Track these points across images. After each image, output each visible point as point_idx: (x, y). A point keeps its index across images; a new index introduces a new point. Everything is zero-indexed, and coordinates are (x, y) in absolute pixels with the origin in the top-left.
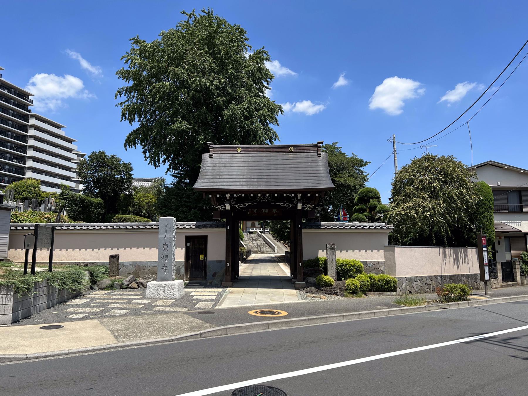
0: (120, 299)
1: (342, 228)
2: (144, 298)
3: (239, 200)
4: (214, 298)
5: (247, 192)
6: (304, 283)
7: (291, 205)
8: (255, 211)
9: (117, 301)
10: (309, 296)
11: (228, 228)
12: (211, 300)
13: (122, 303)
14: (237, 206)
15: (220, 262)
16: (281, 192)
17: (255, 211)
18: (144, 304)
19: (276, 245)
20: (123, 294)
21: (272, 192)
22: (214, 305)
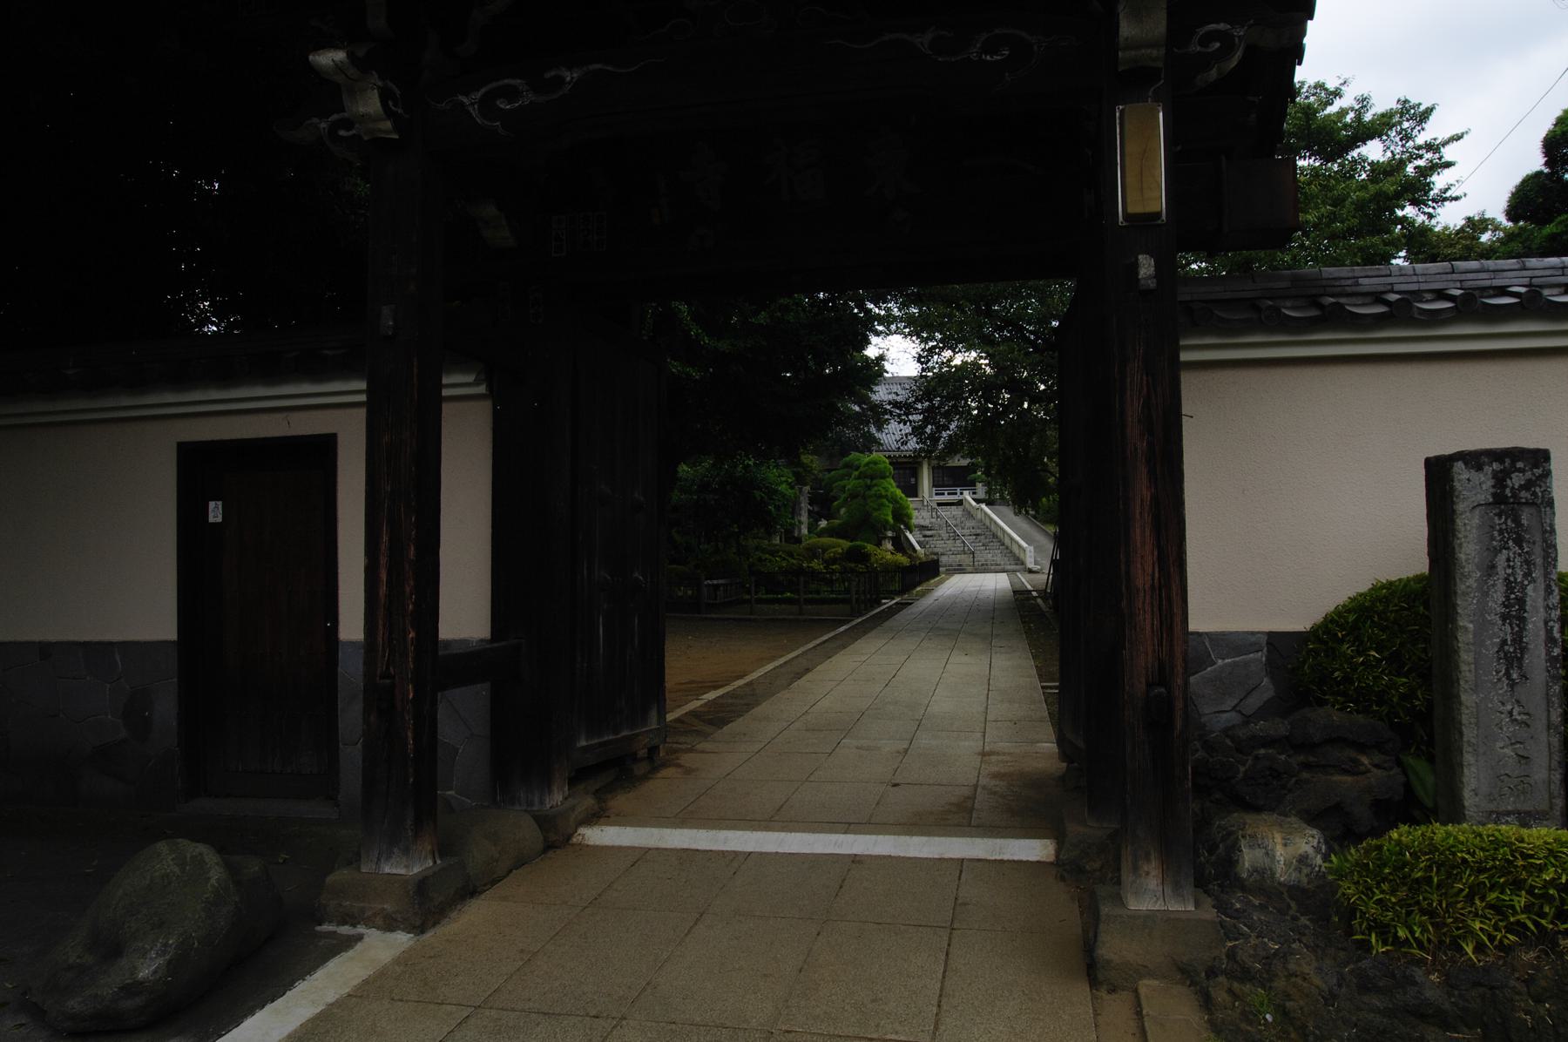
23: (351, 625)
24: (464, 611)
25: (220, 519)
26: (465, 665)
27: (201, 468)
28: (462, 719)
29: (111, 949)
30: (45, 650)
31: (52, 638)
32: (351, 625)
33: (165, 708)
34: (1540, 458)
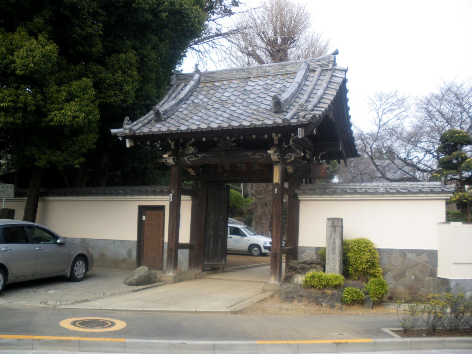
23: (166, 240)
24: (185, 236)
25: (299, 129)
26: (184, 246)
27: (142, 210)
28: (183, 255)
29: (133, 276)
30: (114, 241)
31: (115, 239)
32: (166, 240)
33: (134, 253)
34: (341, 220)
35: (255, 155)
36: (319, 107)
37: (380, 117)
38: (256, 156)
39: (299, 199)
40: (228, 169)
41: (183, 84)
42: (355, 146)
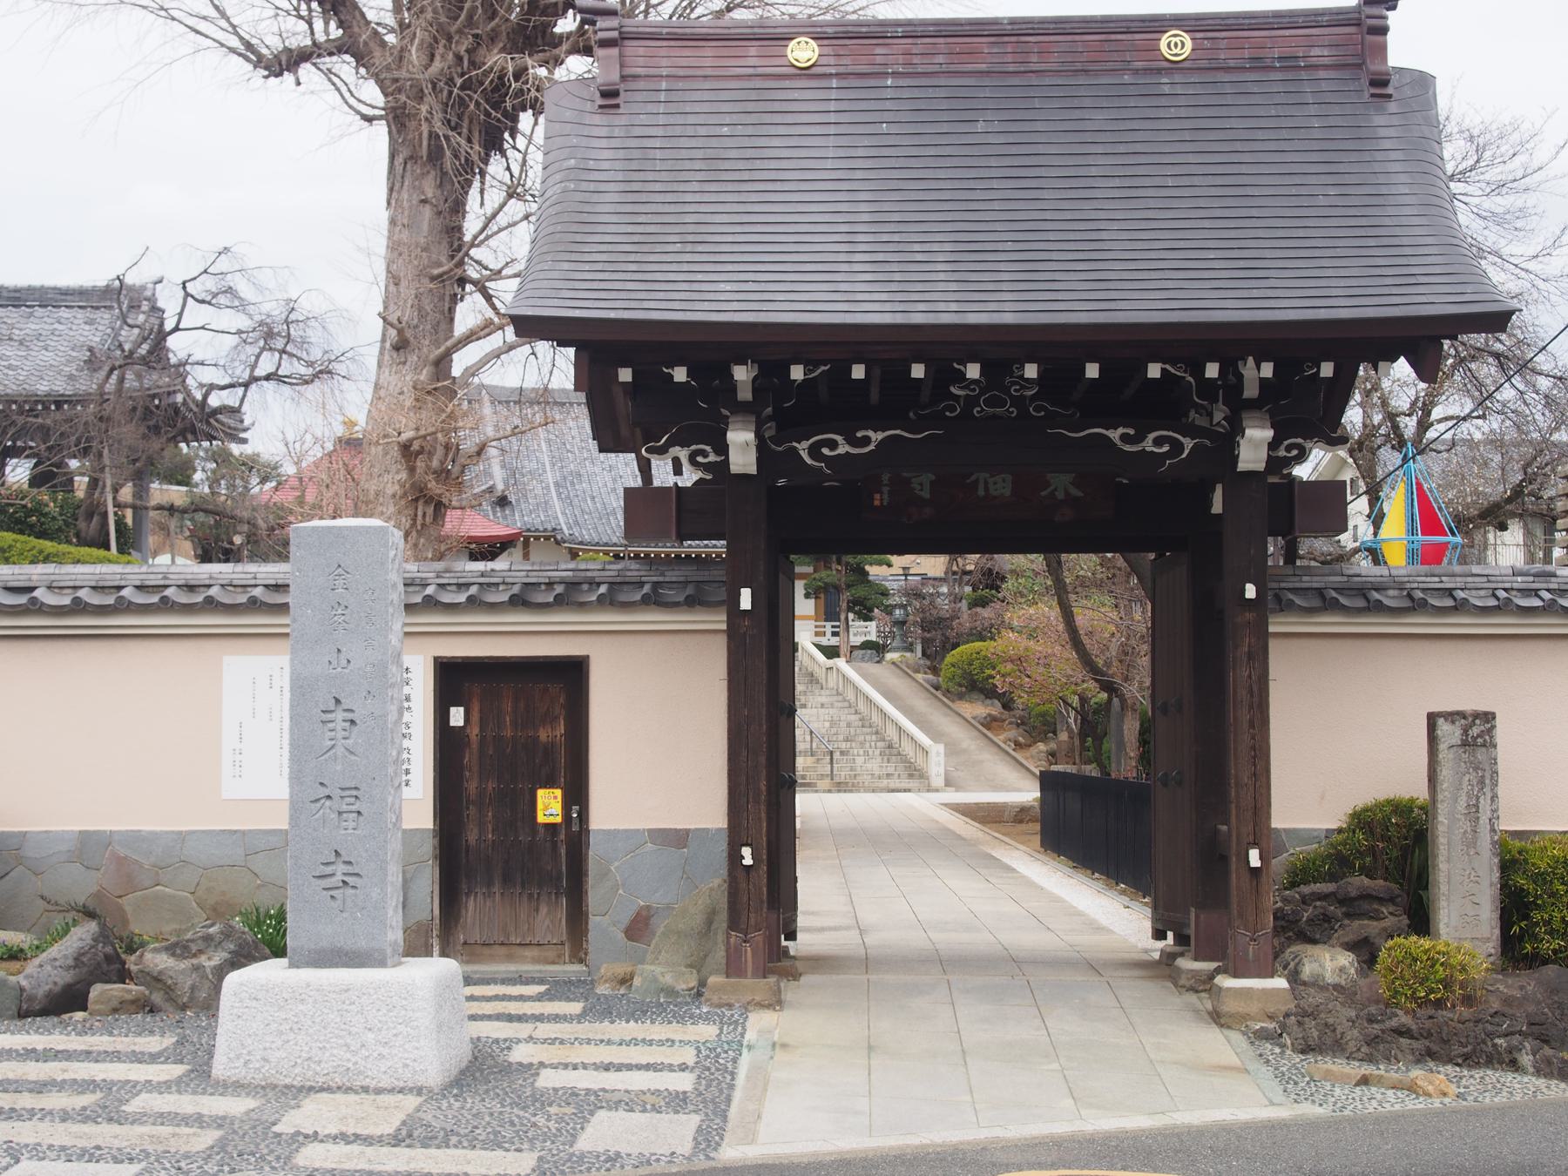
0: (40, 1087)
1: (1537, 603)
2: (201, 1075)
3: (830, 404)
4: (684, 1082)
5: (887, 346)
6: (1280, 983)
7: (1188, 444)
8: (922, 483)
9: (26, 1101)
10: (1328, 1076)
11: (746, 602)
12: (678, 1102)
13: (65, 1116)
14: (803, 448)
15: (677, 839)
16: (1124, 346)
17: (922, 483)
18: (220, 1122)
19: (935, 735)
20: (68, 1055)
21: (1059, 347)
22: (708, 1138)
34: (1489, 717)
35: (1143, 439)
36: (138, 1119)
37: (234, 42)
38: (1148, 445)
39: (1271, 629)
40: (926, 494)
41: (575, 1008)
42: (1479, 332)
